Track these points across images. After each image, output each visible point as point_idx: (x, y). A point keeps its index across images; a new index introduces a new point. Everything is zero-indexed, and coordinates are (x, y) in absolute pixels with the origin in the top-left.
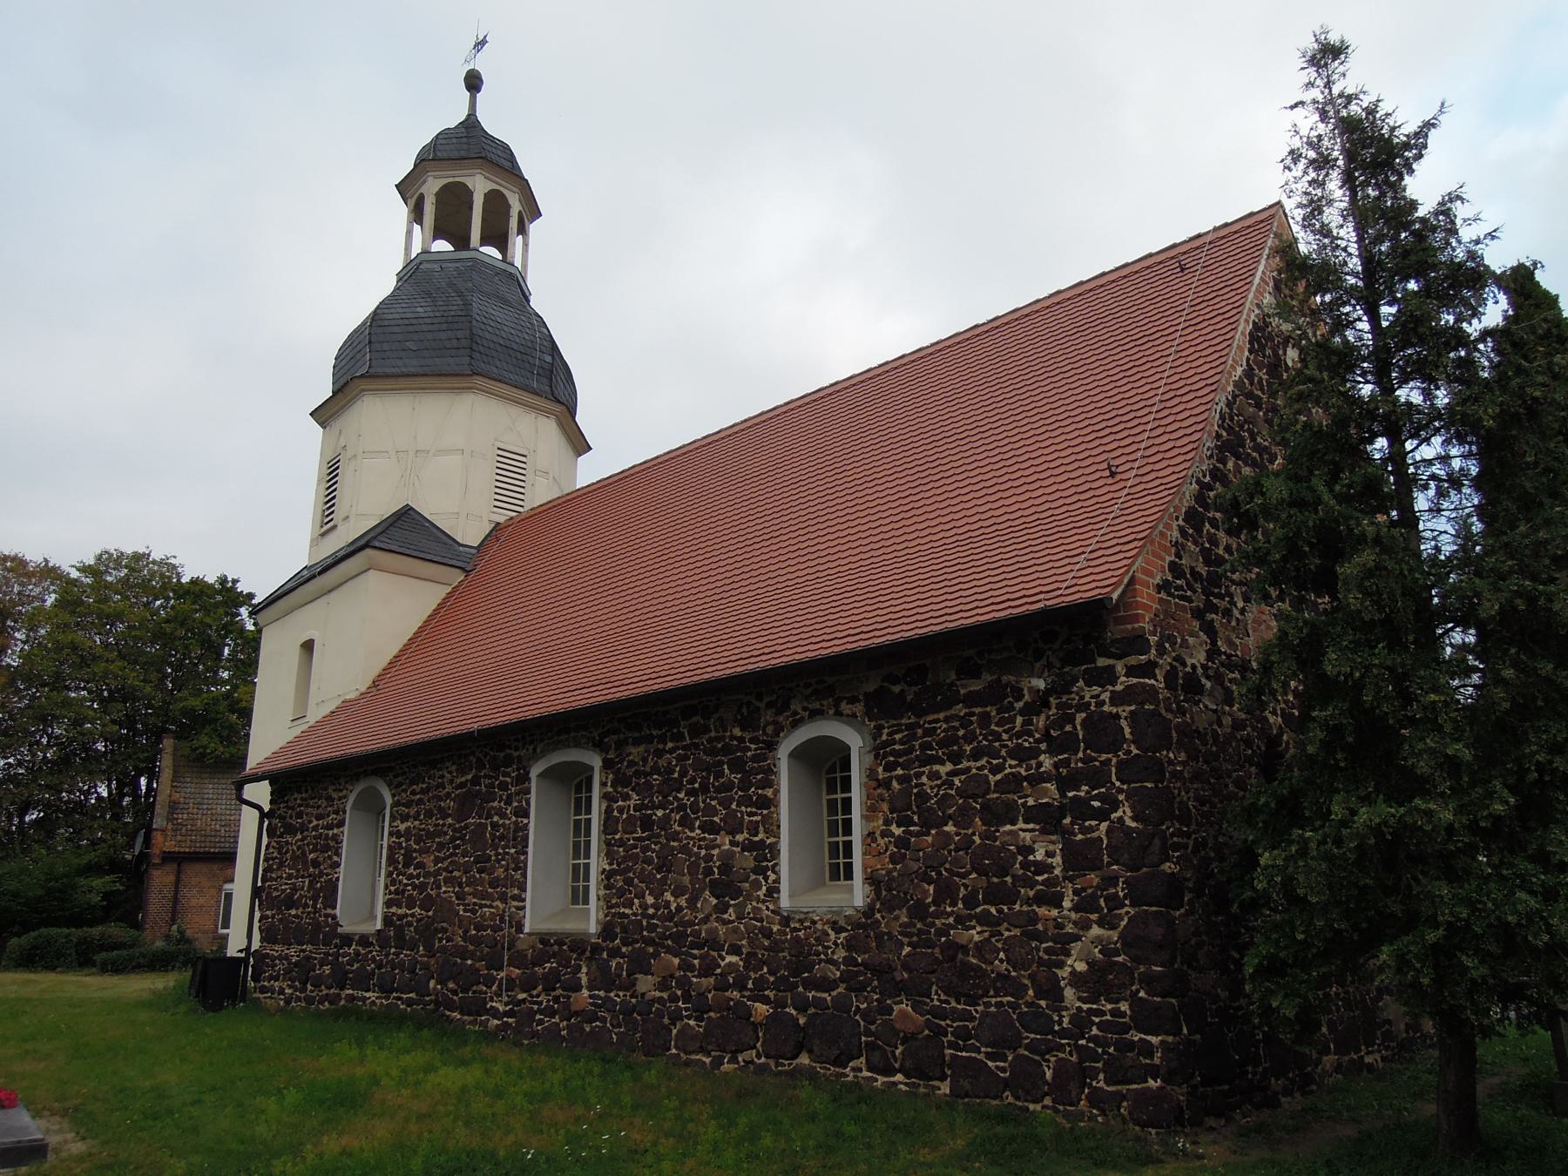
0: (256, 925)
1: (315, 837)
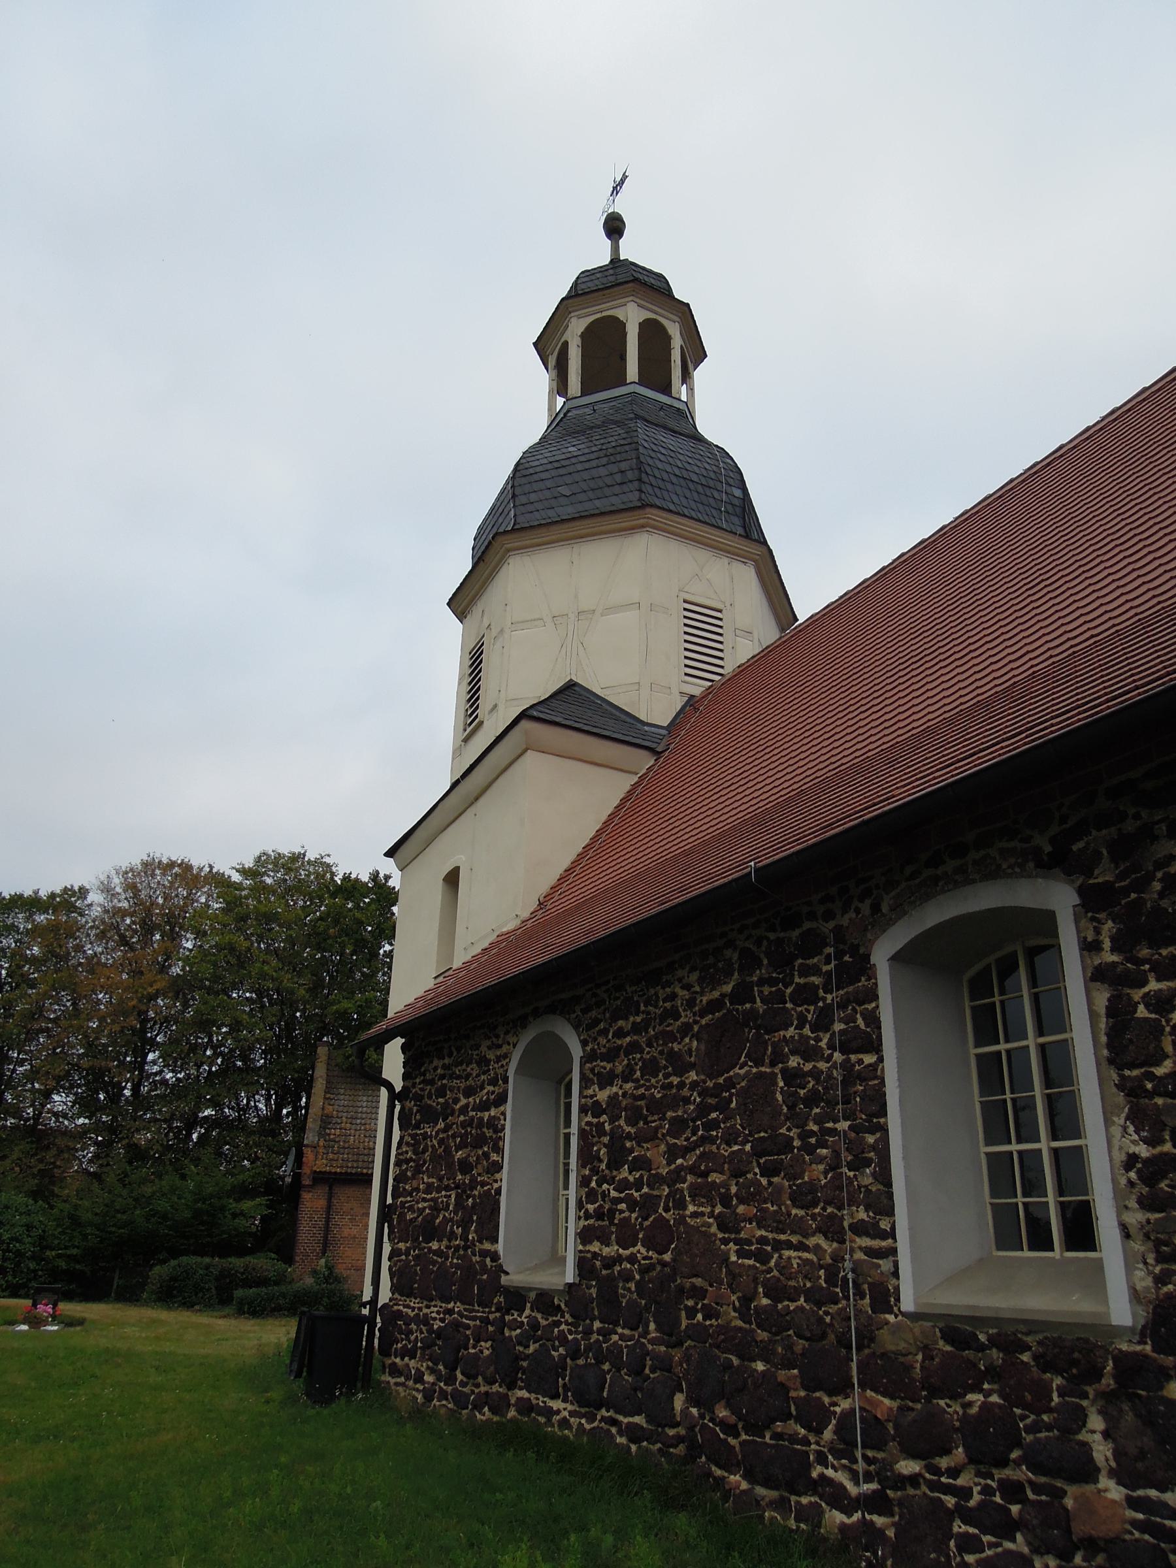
0: (385, 1264)
1: (464, 1125)
